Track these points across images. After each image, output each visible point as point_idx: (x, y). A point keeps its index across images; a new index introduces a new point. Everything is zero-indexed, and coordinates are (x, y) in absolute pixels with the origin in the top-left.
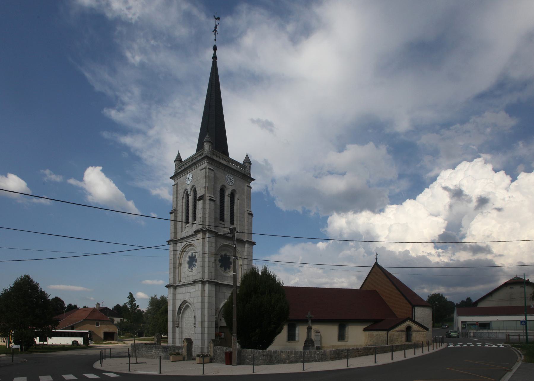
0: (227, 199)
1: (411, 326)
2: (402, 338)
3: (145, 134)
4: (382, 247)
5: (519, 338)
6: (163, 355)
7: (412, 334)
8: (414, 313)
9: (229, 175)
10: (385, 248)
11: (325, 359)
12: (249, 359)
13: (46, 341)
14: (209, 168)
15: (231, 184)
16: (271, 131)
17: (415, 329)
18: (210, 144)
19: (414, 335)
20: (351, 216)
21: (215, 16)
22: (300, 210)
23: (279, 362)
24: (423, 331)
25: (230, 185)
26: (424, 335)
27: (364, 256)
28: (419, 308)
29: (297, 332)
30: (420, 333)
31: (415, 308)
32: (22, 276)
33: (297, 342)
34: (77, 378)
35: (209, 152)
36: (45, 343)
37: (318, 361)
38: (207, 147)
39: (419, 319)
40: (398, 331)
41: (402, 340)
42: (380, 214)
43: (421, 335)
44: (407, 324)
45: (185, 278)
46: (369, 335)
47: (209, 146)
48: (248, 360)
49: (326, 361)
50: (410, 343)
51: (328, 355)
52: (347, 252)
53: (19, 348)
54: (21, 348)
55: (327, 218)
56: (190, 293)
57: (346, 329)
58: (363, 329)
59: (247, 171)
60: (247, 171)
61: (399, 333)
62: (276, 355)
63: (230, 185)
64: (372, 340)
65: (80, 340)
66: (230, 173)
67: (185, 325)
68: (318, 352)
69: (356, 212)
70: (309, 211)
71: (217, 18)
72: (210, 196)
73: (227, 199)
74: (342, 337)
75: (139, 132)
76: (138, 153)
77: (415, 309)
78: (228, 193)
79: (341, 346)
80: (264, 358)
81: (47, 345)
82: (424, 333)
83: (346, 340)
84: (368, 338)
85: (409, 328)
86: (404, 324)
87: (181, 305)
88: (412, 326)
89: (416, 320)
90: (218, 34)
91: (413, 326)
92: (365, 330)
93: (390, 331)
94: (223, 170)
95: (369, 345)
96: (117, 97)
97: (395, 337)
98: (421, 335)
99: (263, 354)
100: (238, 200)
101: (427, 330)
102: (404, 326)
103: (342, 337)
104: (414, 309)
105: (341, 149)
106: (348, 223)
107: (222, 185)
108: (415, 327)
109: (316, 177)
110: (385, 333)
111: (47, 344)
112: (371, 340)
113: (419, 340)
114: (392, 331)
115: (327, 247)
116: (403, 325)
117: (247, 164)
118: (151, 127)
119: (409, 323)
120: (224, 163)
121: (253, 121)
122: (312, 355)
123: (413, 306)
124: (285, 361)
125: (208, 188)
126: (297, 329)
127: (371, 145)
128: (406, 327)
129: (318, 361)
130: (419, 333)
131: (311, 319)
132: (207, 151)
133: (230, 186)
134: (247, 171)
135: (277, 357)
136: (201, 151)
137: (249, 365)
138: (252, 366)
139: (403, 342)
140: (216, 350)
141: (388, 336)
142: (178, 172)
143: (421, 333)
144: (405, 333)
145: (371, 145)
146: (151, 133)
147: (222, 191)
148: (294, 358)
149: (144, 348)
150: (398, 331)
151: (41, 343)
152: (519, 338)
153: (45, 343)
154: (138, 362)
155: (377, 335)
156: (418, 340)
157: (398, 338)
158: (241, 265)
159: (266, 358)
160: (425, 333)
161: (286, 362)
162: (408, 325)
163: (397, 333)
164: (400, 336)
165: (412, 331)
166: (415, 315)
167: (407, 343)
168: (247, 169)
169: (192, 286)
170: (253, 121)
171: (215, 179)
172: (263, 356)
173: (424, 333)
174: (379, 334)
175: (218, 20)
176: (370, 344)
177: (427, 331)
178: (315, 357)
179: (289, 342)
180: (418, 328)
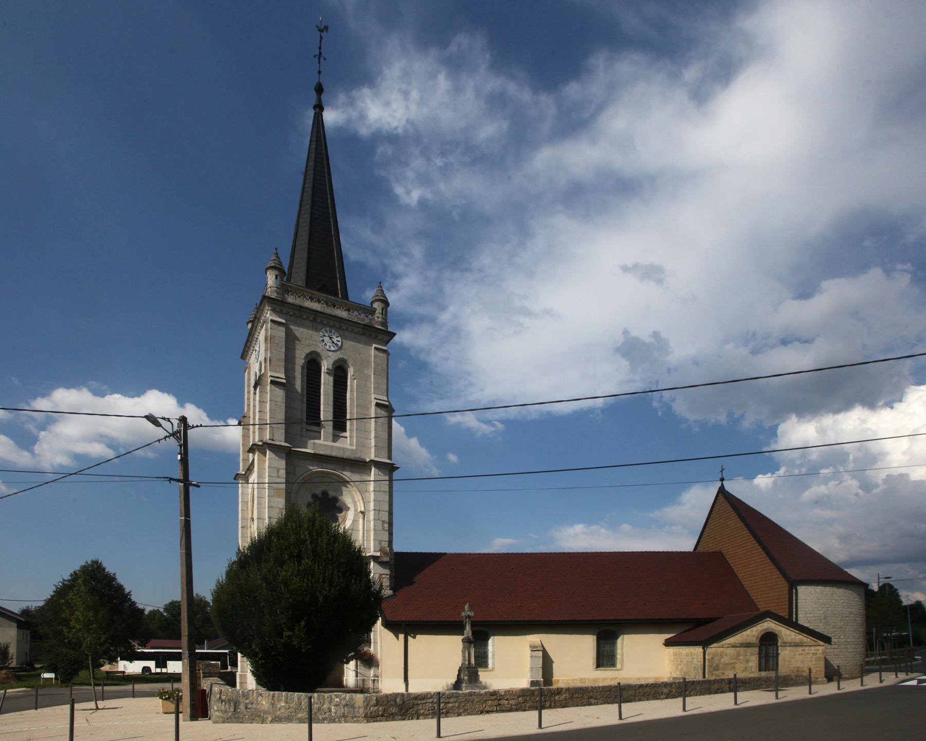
0: (326, 383)
1: (777, 633)
2: (748, 661)
3: (432, 321)
4: (901, 473)
7: (779, 652)
8: (797, 600)
9: (328, 329)
10: (907, 475)
11: (353, 718)
13: (165, 667)
14: (272, 321)
15: (332, 349)
16: (660, 282)
17: (790, 640)
18: (277, 272)
19: (785, 654)
20: (828, 420)
21: (319, 26)
22: (723, 419)
23: (253, 719)
24: (816, 644)
25: (330, 351)
26: (818, 655)
27: (857, 495)
28: (809, 587)
29: (490, 648)
30: (804, 650)
31: (798, 587)
32: (87, 562)
33: (490, 671)
35: (275, 289)
36: (164, 670)
37: (337, 720)
38: (271, 279)
39: (812, 615)
40: (734, 646)
41: (749, 666)
43: (808, 654)
44: (765, 627)
46: (674, 656)
47: (274, 276)
49: (355, 722)
50: (772, 674)
51: (359, 707)
52: (818, 490)
53: (52, 678)
54: (56, 678)
55: (777, 426)
57: (619, 641)
58: (663, 641)
59: (378, 317)
60: (376, 319)
61: (738, 649)
62: (247, 701)
63: (330, 351)
64: (679, 667)
65: (151, 664)
66: (331, 327)
68: (337, 700)
69: (837, 411)
70: (742, 417)
71: (322, 28)
72: (273, 375)
73: (326, 383)
74: (605, 658)
75: (424, 319)
76: (422, 357)
77: (799, 591)
78: (325, 366)
79: (605, 679)
80: (223, 707)
81: (166, 673)
82: (818, 650)
83: (619, 666)
84: (674, 661)
85: (769, 641)
86: (754, 629)
88: (781, 632)
89: (802, 621)
90: (325, 59)
91: (783, 633)
92: (668, 643)
93: (711, 646)
94: (311, 321)
95: (674, 678)
96: (385, 268)
97: (725, 660)
98: (808, 654)
99: (220, 697)
100: (355, 379)
101: (825, 642)
102: (754, 633)
103: (605, 658)
104: (794, 591)
105: (805, 292)
106: (822, 431)
107: (310, 351)
108: (786, 633)
109: (753, 352)
110: (699, 650)
111: (166, 672)
112: (677, 667)
113: (801, 666)
114: (715, 645)
115: (775, 483)
116: (752, 631)
117: (376, 303)
118: (443, 308)
119: (769, 625)
120: (343, 314)
121: (625, 269)
122: (325, 706)
123: (793, 584)
124: (265, 716)
125: (270, 360)
126: (490, 642)
127: (876, 273)
128: (760, 636)
129: (337, 720)
130: (800, 649)
131: (472, 622)
132: (271, 287)
133: (330, 353)
134: (376, 319)
135: (250, 706)
138: (306, 726)
139: (752, 672)
141: (707, 657)
143: (807, 648)
144: (757, 649)
145: (876, 273)
146: (444, 317)
147: (313, 364)
148: (283, 710)
150: (734, 646)
151: (158, 670)
153: (164, 670)
154: (99, 708)
155: (687, 656)
156: (798, 667)
157: (734, 663)
158: (362, 512)
159: (227, 706)
160: (820, 648)
161: (267, 718)
162: (767, 629)
163: (731, 651)
164: (741, 657)
165: (779, 644)
166: (799, 604)
167: (763, 674)
168: (376, 315)
170: (625, 269)
171: (291, 341)
172: (222, 703)
173: (818, 650)
174: (691, 653)
175: (325, 31)
176: (675, 676)
177: (826, 645)
178: (330, 710)
179: (599, 669)
180: (800, 637)
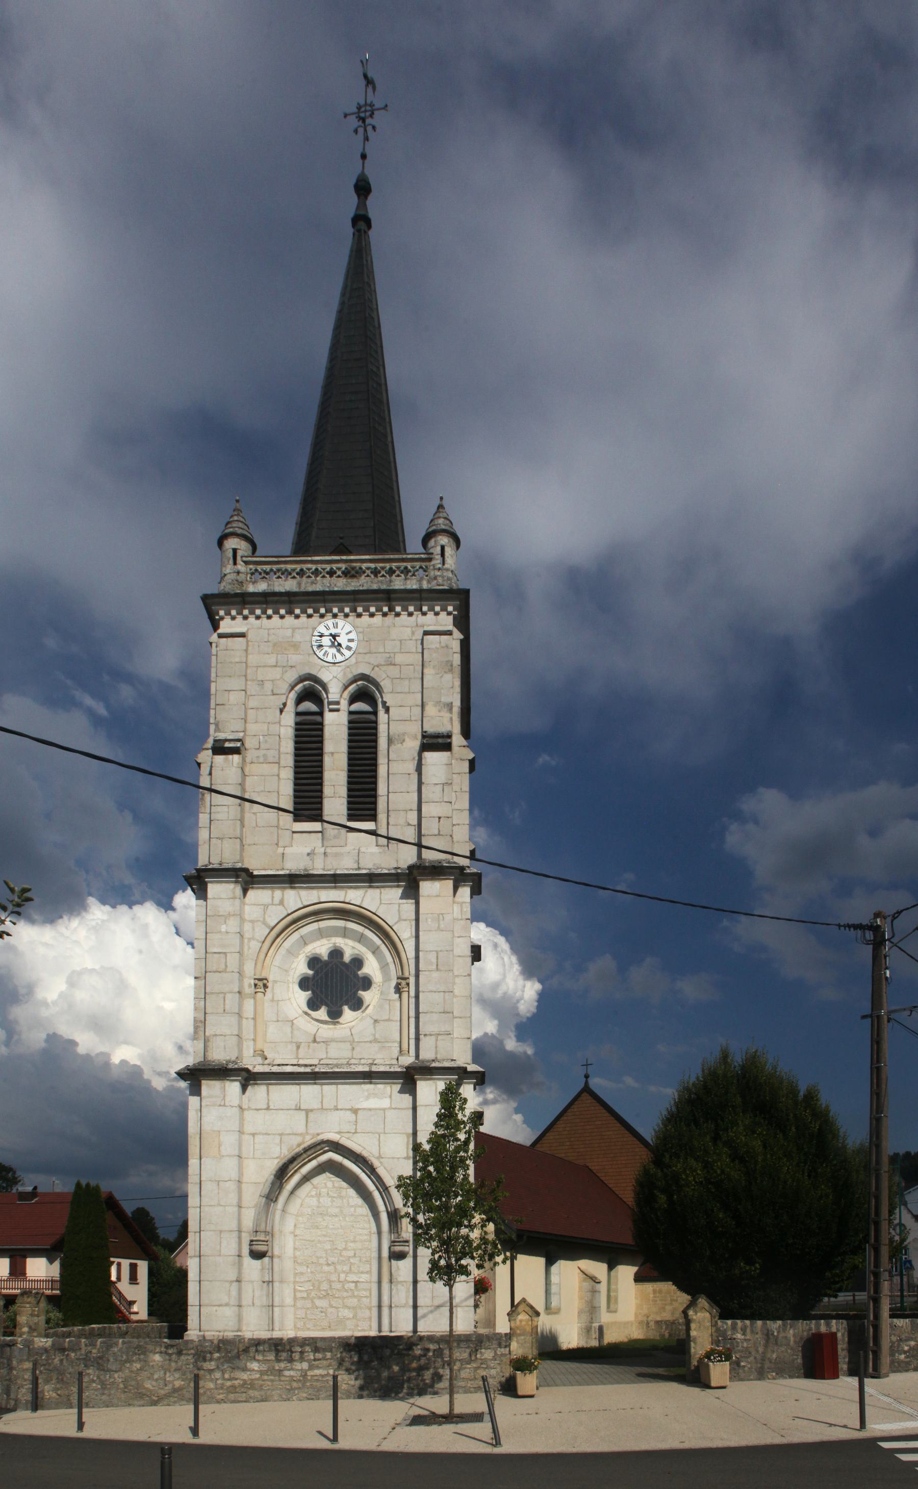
5: (854, 1300)
6: (348, 1381)
12: (905, 1352)
34: (879, 1443)
37: (416, 1392)
42: (166, 912)
45: (298, 1047)
48: (902, 1357)
56: (355, 1111)
64: (668, 1308)
67: (295, 1249)
87: (292, 1160)
112: (664, 1308)
136: (367, 557)
137: (907, 1371)
140: (729, 1333)
142: (251, 589)
149: (157, 1357)
152: (854, 1300)
169: (371, 1083)
